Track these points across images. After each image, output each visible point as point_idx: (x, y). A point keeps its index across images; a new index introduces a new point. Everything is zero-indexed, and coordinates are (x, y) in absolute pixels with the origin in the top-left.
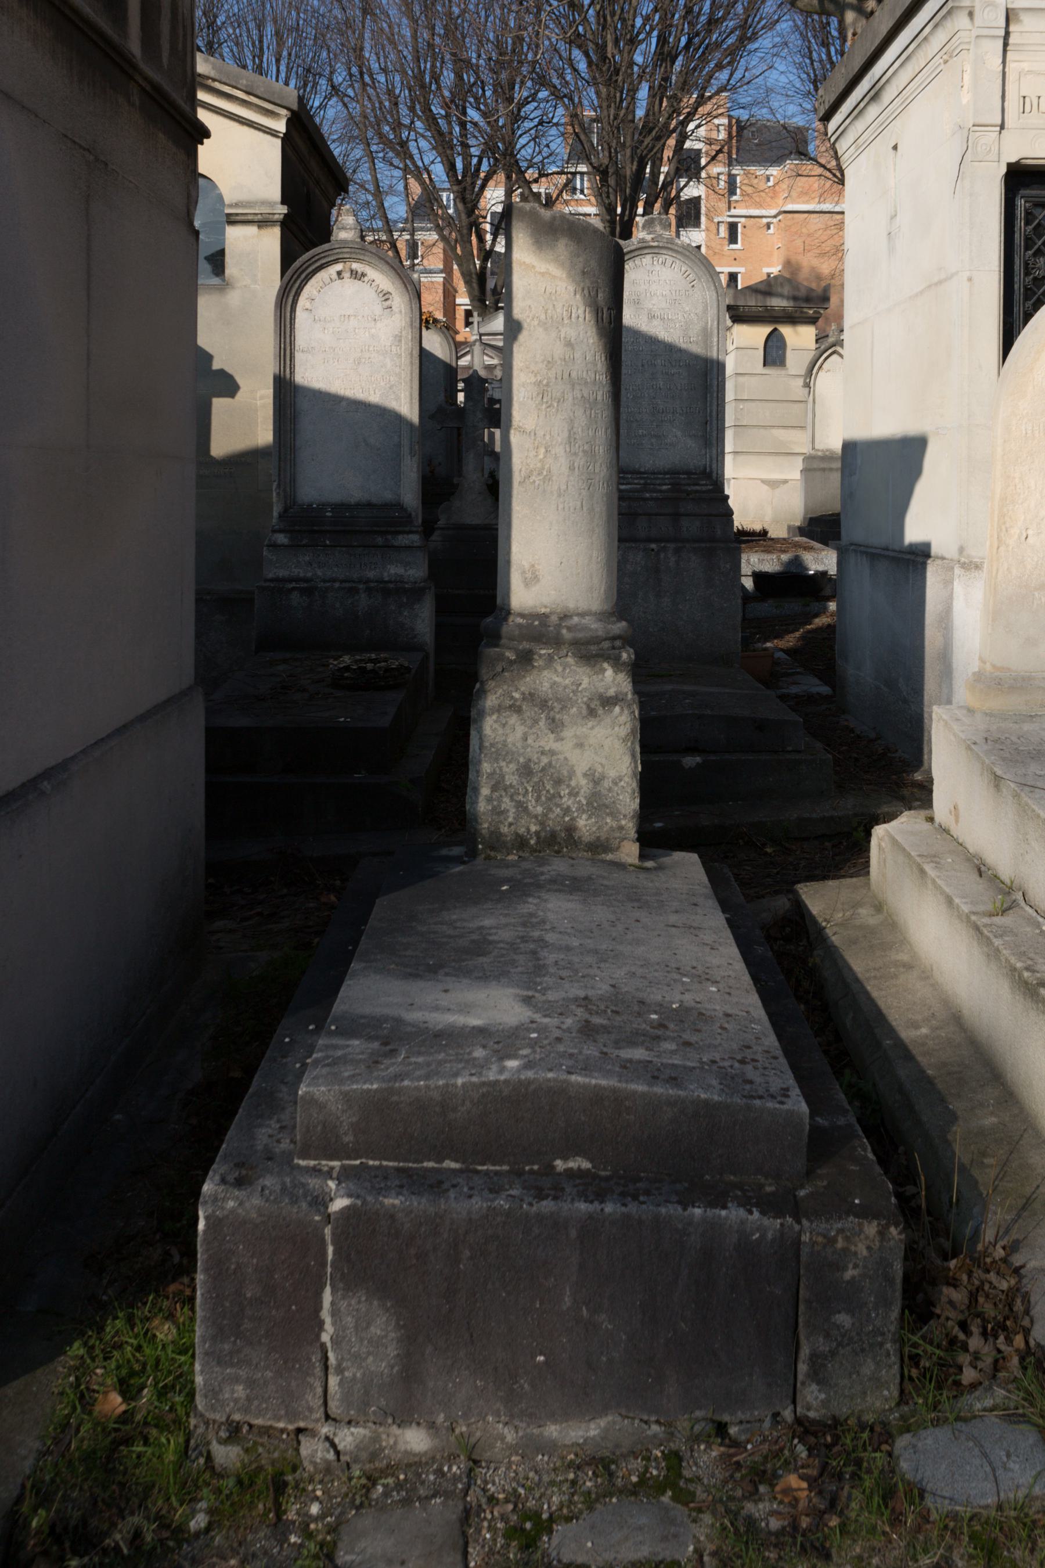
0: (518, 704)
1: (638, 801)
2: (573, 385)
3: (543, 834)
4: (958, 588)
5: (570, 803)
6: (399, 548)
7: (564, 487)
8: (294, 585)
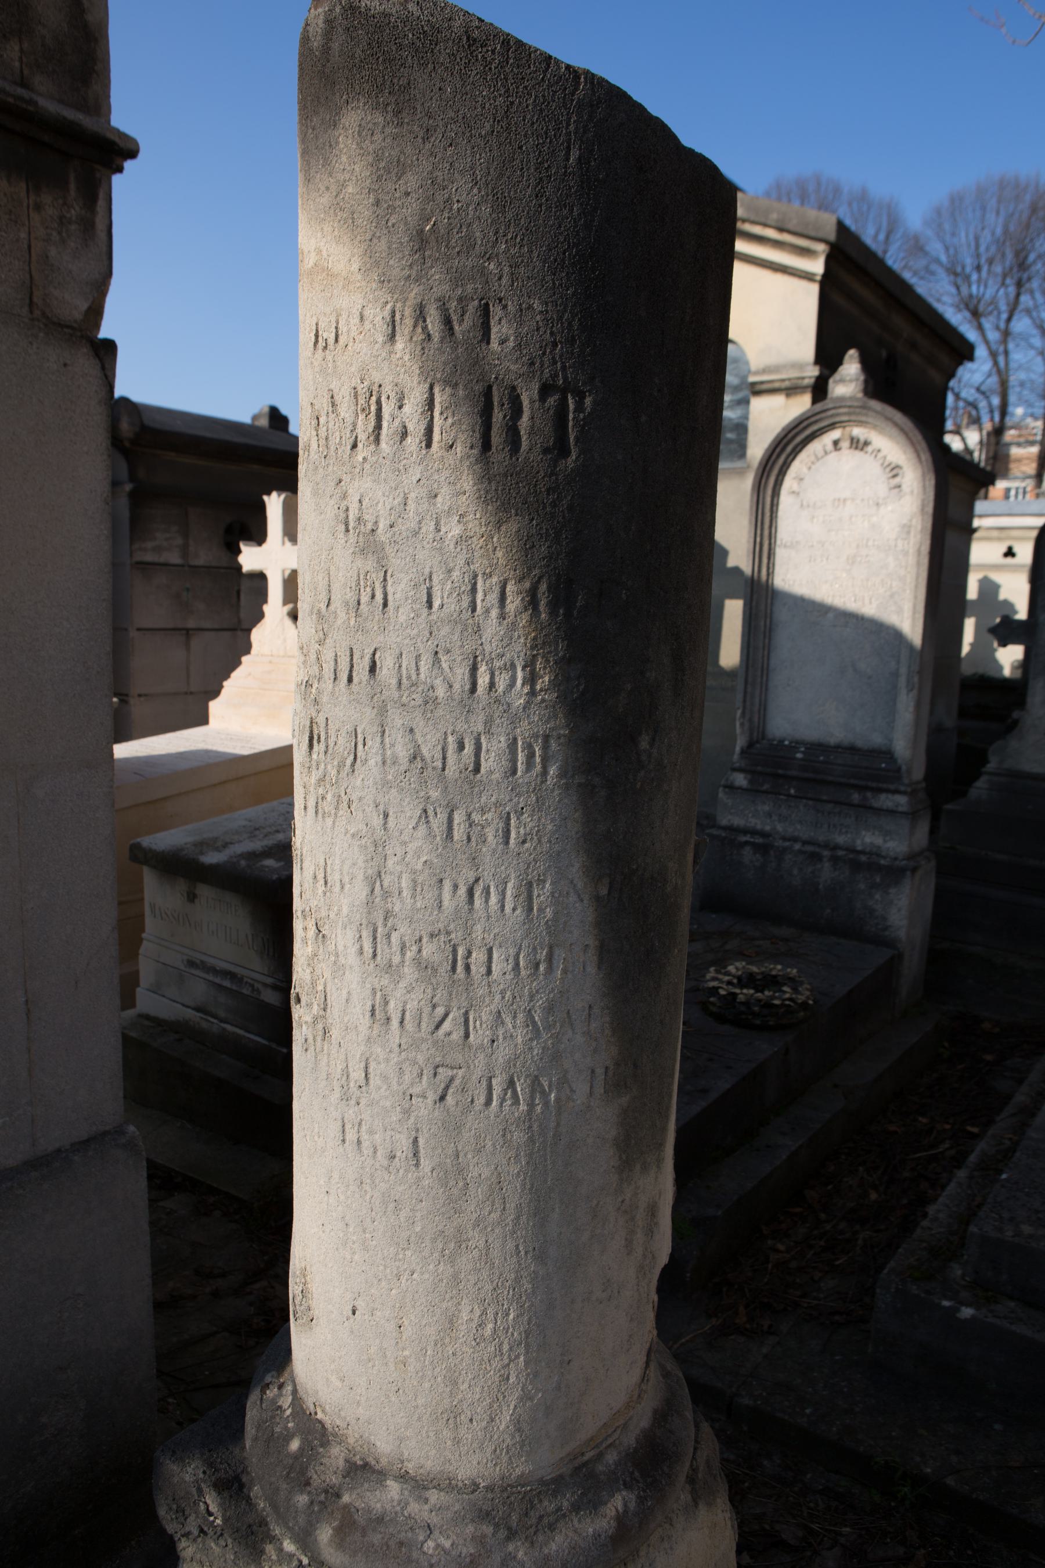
6: (879, 811)
8: (747, 838)
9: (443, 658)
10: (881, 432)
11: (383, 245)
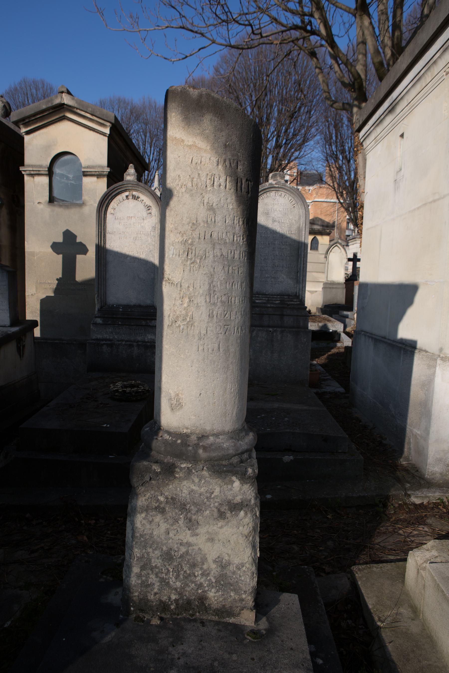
0: (162, 506)
1: (256, 579)
2: (214, 245)
3: (181, 602)
4: (438, 371)
5: (202, 580)
7: (203, 332)
8: (104, 342)
9: (228, 234)
10: (143, 194)
11: (217, 145)
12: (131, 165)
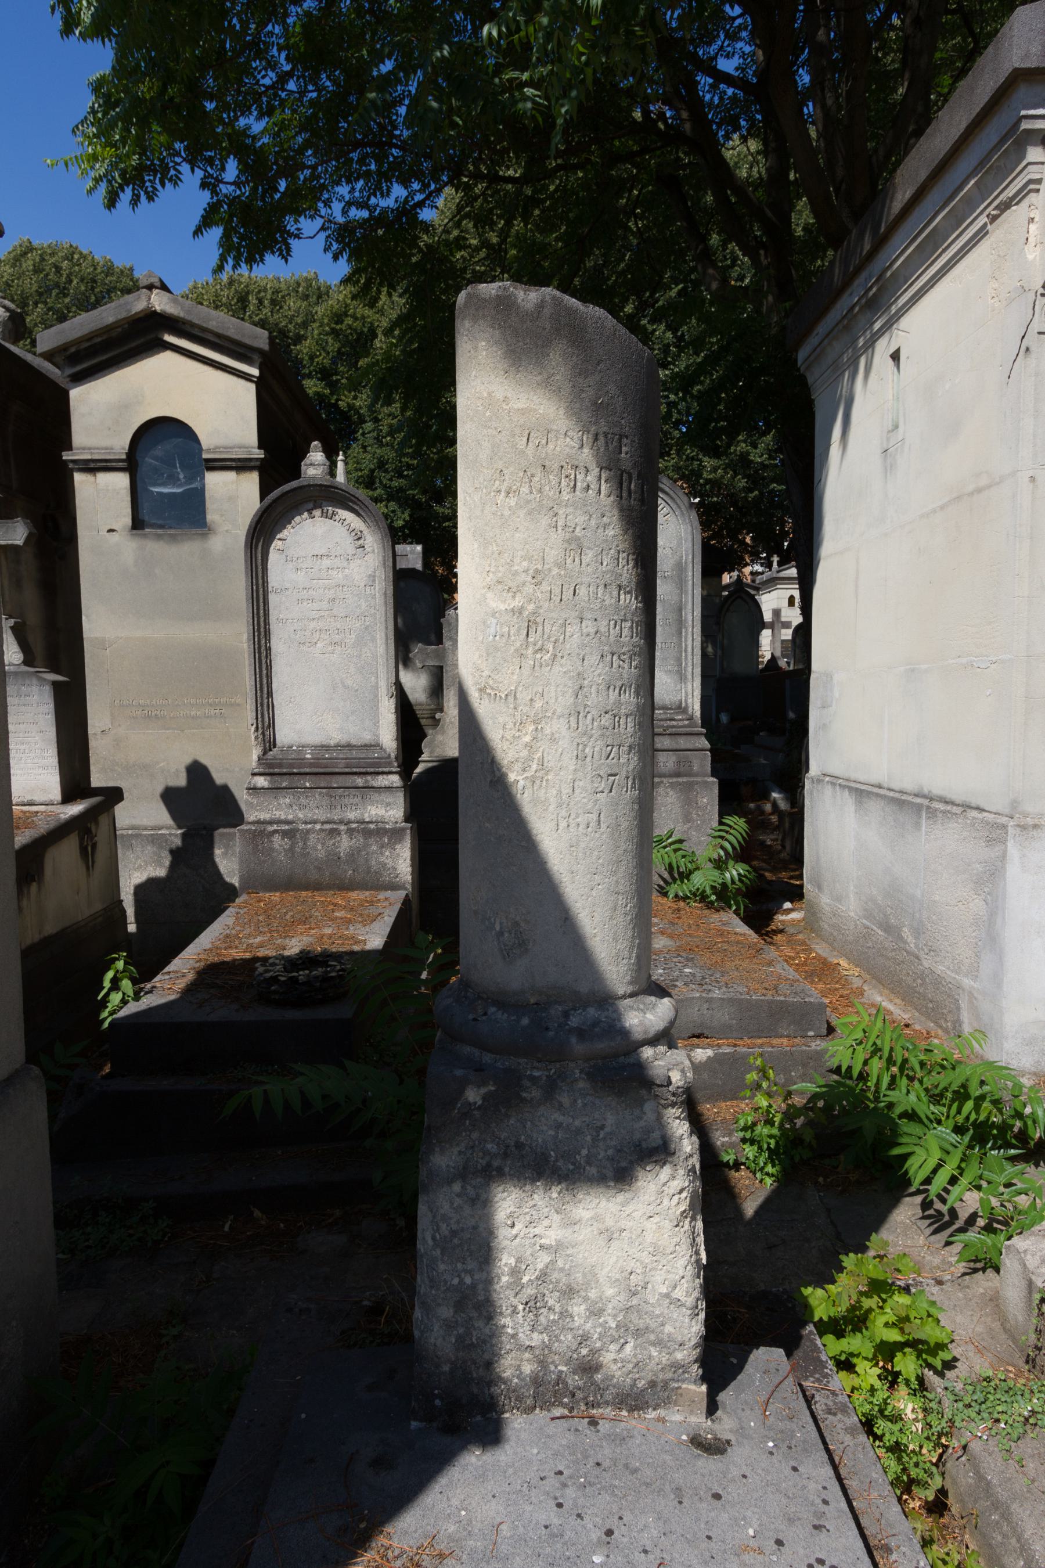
4: (1013, 849)
7: (566, 790)
8: (275, 827)
11: (578, 405)
12: (316, 443)
